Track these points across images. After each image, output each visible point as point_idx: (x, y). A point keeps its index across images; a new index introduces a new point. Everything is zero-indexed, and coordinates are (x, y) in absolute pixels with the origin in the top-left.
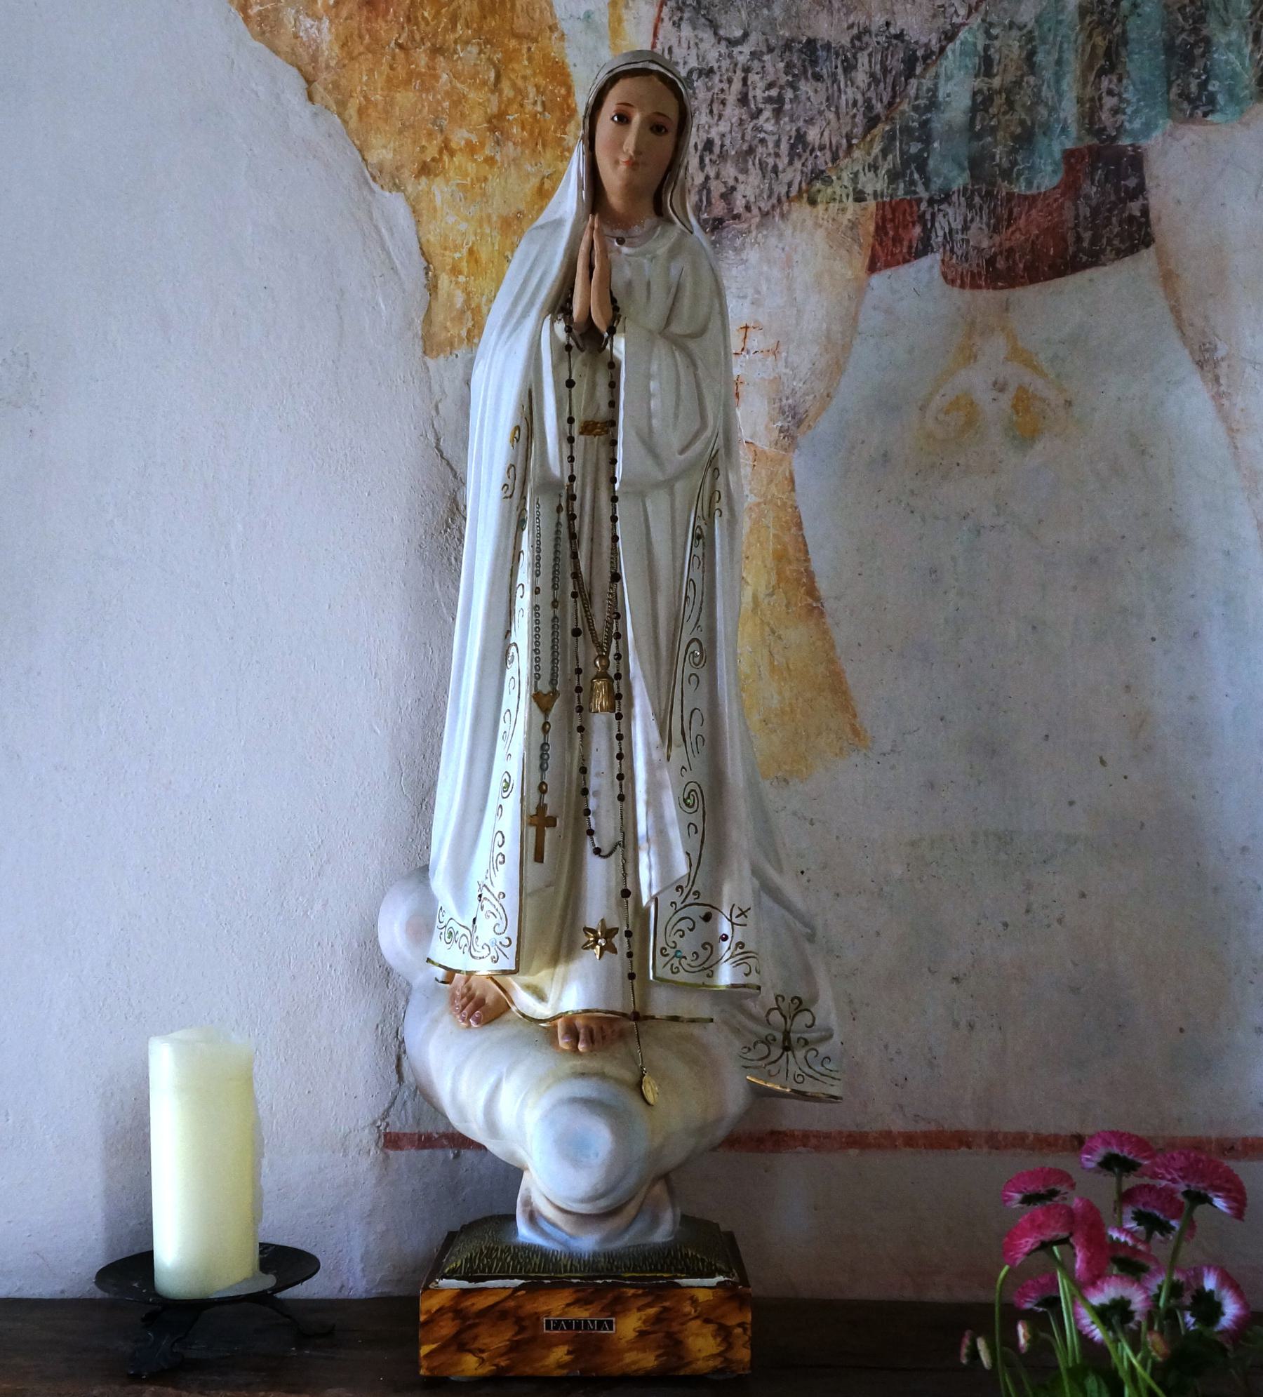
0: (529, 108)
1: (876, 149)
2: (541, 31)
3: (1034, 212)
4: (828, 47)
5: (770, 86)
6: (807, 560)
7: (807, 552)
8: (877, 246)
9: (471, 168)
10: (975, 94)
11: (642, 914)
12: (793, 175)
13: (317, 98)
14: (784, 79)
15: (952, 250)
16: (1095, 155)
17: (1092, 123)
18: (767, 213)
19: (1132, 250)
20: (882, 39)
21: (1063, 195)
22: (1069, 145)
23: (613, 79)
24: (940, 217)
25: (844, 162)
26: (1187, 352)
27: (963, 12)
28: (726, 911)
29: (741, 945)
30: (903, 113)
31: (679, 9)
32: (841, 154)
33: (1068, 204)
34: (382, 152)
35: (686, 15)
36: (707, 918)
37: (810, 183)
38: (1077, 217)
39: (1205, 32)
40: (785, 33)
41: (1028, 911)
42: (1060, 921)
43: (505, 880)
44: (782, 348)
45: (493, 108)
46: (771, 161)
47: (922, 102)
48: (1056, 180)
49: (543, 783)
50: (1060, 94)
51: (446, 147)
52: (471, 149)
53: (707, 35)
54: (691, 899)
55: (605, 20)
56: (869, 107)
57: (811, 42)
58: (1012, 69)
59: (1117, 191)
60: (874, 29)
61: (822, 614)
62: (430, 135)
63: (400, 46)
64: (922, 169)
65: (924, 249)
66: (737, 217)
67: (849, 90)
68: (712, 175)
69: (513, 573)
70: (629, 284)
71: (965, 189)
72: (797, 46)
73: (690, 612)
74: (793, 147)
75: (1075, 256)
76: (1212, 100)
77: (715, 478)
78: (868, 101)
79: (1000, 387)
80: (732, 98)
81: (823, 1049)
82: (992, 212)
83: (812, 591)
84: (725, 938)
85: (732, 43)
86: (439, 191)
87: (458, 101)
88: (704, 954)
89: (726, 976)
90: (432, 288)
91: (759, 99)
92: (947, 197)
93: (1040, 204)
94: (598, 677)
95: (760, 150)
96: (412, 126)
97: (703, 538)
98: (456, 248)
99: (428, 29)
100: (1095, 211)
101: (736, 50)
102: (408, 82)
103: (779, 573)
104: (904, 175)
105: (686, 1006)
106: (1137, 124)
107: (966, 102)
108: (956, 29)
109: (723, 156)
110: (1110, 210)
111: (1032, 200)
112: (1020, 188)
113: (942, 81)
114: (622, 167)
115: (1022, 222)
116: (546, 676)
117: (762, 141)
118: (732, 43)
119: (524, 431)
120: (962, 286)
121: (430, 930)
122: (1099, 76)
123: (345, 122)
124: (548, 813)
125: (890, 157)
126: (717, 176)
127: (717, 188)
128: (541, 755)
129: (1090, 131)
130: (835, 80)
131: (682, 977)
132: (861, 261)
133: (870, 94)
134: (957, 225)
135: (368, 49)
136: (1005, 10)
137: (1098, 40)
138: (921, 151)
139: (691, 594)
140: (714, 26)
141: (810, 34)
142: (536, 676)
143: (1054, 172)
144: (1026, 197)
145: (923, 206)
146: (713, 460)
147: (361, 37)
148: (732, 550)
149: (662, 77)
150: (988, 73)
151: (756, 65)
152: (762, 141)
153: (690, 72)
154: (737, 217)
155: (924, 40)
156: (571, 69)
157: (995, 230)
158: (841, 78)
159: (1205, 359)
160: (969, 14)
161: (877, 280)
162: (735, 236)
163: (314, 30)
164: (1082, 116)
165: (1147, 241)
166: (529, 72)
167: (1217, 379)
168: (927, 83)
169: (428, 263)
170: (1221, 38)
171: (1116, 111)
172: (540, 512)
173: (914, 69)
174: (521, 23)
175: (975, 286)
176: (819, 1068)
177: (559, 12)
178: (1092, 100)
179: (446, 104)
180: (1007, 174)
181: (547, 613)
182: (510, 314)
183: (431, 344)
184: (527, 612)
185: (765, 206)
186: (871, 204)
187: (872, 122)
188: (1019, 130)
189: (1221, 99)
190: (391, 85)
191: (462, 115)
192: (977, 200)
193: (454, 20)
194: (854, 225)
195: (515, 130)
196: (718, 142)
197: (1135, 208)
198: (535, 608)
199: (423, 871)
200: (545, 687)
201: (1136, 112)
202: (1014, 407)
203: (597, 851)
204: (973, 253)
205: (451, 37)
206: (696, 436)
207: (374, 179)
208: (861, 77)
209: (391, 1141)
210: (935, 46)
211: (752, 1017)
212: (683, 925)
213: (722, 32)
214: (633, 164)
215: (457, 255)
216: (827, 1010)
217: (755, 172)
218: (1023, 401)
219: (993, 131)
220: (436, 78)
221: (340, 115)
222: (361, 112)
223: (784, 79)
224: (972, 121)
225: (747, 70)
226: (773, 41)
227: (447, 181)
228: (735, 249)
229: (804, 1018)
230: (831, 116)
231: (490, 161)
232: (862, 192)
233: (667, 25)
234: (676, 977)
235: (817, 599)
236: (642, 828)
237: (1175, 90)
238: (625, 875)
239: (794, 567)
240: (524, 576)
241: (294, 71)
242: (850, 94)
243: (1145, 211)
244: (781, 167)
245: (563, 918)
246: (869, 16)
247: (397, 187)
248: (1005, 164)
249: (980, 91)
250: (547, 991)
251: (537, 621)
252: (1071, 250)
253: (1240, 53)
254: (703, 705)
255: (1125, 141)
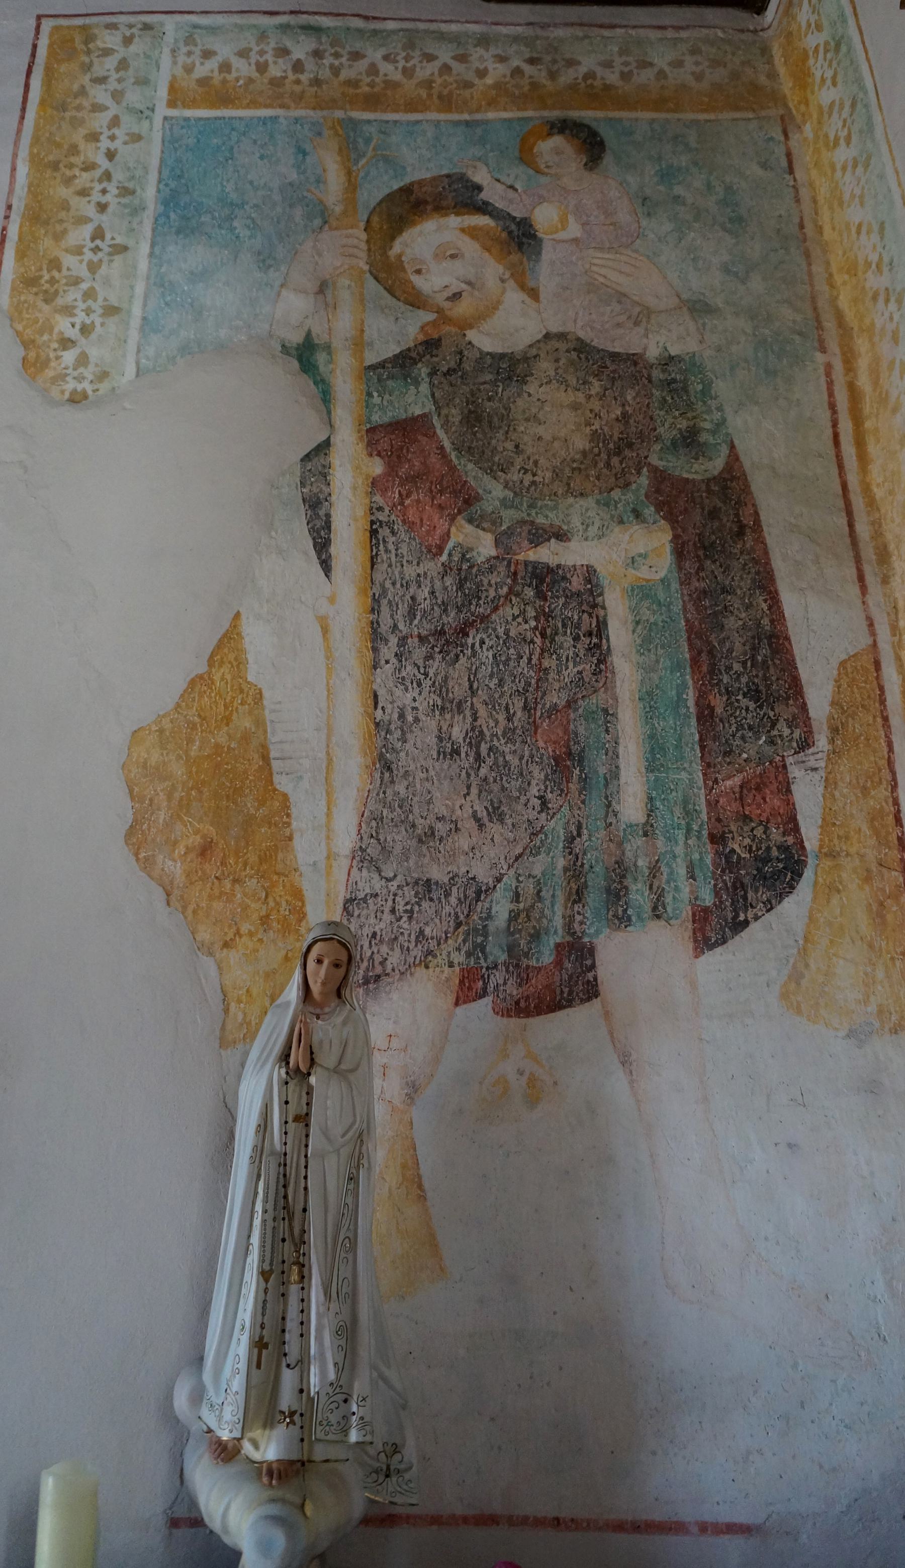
0: (282, 912)
1: (460, 940)
2: (289, 872)
3: (539, 976)
4: (437, 883)
5: (407, 904)
6: (419, 1169)
7: (418, 1164)
8: (460, 992)
9: (250, 945)
10: (510, 912)
11: (311, 1400)
12: (417, 952)
13: (171, 904)
14: (414, 900)
15: (498, 996)
16: (571, 946)
17: (569, 929)
18: (403, 973)
19: (589, 999)
20: (464, 880)
21: (554, 967)
22: (558, 940)
23: (315, 942)
24: (492, 977)
25: (442, 947)
26: (616, 1056)
27: (505, 867)
28: (355, 1397)
29: (362, 1418)
30: (474, 920)
31: (362, 861)
32: (442, 942)
33: (557, 973)
34: (205, 934)
35: (365, 865)
36: (346, 1401)
37: (426, 957)
38: (561, 980)
39: (625, 884)
40: (415, 875)
41: (531, 1377)
42: (548, 1384)
43: (238, 1384)
44: (408, 1048)
45: (263, 913)
46: (406, 944)
47: (484, 915)
48: (551, 959)
49: (263, 1323)
50: (554, 913)
51: (238, 933)
52: (251, 934)
53: (376, 876)
54: (338, 1390)
55: (323, 867)
56: (457, 917)
57: (428, 880)
58: (529, 900)
59: (581, 967)
60: (460, 875)
61: (425, 1199)
62: (230, 926)
63: (217, 878)
64: (483, 952)
65: (484, 994)
66: (387, 975)
67: (447, 907)
68: (376, 951)
69: (254, 1204)
70: (321, 1042)
71: (505, 962)
72: (421, 883)
73: (346, 1222)
74: (417, 937)
75: (560, 1001)
76: (629, 919)
77: (361, 1146)
78: (456, 914)
79: (521, 1073)
80: (387, 910)
81: (407, 1476)
82: (519, 975)
83: (420, 1186)
84: (354, 1414)
85: (388, 880)
86: (233, 956)
87: (245, 908)
88: (343, 1423)
89: (354, 1436)
90: (226, 1011)
91: (401, 911)
92: (496, 967)
93: (542, 971)
94: (294, 1264)
95: (400, 938)
96: (221, 921)
97: (353, 1179)
98: (240, 988)
99: (232, 869)
100: (570, 977)
101: (390, 884)
102: (220, 897)
103: (404, 1176)
104: (474, 954)
105: (334, 1452)
106: (592, 931)
107: (506, 916)
108: (502, 875)
109: (381, 941)
110: (578, 977)
111: (539, 969)
112: (533, 963)
113: (494, 904)
114: (319, 984)
115: (533, 981)
116: (268, 1262)
117: (402, 933)
118: (388, 880)
119: (262, 1127)
120: (503, 1016)
121: (201, 1400)
122: (573, 904)
123: (186, 918)
124: (265, 1341)
125: (467, 944)
126: (378, 952)
127: (378, 959)
128: (262, 1306)
129: (568, 933)
130: (440, 902)
131: (331, 1437)
132: (451, 999)
133: (458, 910)
134: (501, 982)
135: (201, 879)
136: (527, 868)
137: (573, 885)
138: (483, 941)
139: (346, 1212)
140: (379, 870)
141: (428, 876)
142: (262, 1260)
143: (550, 955)
144: (536, 968)
145: (484, 970)
146: (361, 1134)
147: (196, 872)
148: (369, 1179)
149: (339, 942)
150: (518, 901)
151: (400, 892)
152: (402, 933)
153: (366, 895)
154: (387, 975)
155: (485, 881)
156: (305, 892)
157: (520, 985)
158: (443, 900)
159: (625, 1061)
160: (509, 868)
161: (460, 1010)
162: (386, 985)
163: (172, 867)
164: (565, 925)
165: (596, 995)
166: (283, 893)
167: (631, 1072)
168: (487, 905)
169: (225, 996)
170: (633, 887)
171: (581, 923)
172: (270, 1168)
173: (480, 896)
174: (280, 867)
175: (510, 1016)
176: (405, 1487)
177: (300, 861)
178: (570, 916)
179: (239, 910)
180: (526, 955)
181: (270, 1224)
182: (259, 1059)
183: (224, 1043)
184: (259, 1227)
185: (402, 969)
186: (457, 969)
187: (459, 925)
188: (532, 932)
189: (634, 919)
190: (211, 898)
191: (247, 916)
192: (511, 968)
193: (245, 864)
194: (448, 980)
195: (275, 924)
196: (379, 933)
197: (590, 976)
198: (264, 1221)
199: (200, 1360)
200: (267, 1267)
201: (592, 923)
202: (528, 1084)
203: (288, 1366)
204: (509, 998)
205: (244, 873)
206: (351, 1127)
207: (199, 949)
208: (453, 900)
209: (174, 1523)
210: (491, 885)
211: (369, 1456)
212: (332, 1406)
213: (383, 874)
214: (324, 984)
215: (241, 992)
216: (410, 1452)
217: (397, 950)
218: (532, 1081)
219: (520, 931)
220: (234, 895)
221: (183, 913)
222: (194, 912)
223: (414, 900)
224: (509, 926)
225: (395, 895)
226: (409, 880)
227: (238, 951)
228: (386, 992)
229: (398, 1457)
230: (437, 921)
231: (261, 941)
232: (452, 962)
233: (355, 870)
234: (328, 1438)
235: (423, 1190)
236: (312, 1352)
237: (611, 913)
238: (302, 1380)
239: (411, 1173)
240: (259, 1207)
241: (161, 889)
242: (448, 909)
243: (595, 979)
244: (411, 948)
245: (270, 1403)
246: (459, 868)
247: (211, 954)
248: (526, 950)
249: (513, 910)
250: (260, 1443)
251: (265, 1229)
252: (558, 998)
253: (643, 894)
254: (349, 1275)
255: (586, 940)
